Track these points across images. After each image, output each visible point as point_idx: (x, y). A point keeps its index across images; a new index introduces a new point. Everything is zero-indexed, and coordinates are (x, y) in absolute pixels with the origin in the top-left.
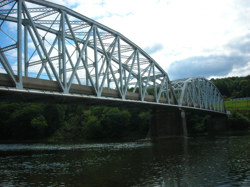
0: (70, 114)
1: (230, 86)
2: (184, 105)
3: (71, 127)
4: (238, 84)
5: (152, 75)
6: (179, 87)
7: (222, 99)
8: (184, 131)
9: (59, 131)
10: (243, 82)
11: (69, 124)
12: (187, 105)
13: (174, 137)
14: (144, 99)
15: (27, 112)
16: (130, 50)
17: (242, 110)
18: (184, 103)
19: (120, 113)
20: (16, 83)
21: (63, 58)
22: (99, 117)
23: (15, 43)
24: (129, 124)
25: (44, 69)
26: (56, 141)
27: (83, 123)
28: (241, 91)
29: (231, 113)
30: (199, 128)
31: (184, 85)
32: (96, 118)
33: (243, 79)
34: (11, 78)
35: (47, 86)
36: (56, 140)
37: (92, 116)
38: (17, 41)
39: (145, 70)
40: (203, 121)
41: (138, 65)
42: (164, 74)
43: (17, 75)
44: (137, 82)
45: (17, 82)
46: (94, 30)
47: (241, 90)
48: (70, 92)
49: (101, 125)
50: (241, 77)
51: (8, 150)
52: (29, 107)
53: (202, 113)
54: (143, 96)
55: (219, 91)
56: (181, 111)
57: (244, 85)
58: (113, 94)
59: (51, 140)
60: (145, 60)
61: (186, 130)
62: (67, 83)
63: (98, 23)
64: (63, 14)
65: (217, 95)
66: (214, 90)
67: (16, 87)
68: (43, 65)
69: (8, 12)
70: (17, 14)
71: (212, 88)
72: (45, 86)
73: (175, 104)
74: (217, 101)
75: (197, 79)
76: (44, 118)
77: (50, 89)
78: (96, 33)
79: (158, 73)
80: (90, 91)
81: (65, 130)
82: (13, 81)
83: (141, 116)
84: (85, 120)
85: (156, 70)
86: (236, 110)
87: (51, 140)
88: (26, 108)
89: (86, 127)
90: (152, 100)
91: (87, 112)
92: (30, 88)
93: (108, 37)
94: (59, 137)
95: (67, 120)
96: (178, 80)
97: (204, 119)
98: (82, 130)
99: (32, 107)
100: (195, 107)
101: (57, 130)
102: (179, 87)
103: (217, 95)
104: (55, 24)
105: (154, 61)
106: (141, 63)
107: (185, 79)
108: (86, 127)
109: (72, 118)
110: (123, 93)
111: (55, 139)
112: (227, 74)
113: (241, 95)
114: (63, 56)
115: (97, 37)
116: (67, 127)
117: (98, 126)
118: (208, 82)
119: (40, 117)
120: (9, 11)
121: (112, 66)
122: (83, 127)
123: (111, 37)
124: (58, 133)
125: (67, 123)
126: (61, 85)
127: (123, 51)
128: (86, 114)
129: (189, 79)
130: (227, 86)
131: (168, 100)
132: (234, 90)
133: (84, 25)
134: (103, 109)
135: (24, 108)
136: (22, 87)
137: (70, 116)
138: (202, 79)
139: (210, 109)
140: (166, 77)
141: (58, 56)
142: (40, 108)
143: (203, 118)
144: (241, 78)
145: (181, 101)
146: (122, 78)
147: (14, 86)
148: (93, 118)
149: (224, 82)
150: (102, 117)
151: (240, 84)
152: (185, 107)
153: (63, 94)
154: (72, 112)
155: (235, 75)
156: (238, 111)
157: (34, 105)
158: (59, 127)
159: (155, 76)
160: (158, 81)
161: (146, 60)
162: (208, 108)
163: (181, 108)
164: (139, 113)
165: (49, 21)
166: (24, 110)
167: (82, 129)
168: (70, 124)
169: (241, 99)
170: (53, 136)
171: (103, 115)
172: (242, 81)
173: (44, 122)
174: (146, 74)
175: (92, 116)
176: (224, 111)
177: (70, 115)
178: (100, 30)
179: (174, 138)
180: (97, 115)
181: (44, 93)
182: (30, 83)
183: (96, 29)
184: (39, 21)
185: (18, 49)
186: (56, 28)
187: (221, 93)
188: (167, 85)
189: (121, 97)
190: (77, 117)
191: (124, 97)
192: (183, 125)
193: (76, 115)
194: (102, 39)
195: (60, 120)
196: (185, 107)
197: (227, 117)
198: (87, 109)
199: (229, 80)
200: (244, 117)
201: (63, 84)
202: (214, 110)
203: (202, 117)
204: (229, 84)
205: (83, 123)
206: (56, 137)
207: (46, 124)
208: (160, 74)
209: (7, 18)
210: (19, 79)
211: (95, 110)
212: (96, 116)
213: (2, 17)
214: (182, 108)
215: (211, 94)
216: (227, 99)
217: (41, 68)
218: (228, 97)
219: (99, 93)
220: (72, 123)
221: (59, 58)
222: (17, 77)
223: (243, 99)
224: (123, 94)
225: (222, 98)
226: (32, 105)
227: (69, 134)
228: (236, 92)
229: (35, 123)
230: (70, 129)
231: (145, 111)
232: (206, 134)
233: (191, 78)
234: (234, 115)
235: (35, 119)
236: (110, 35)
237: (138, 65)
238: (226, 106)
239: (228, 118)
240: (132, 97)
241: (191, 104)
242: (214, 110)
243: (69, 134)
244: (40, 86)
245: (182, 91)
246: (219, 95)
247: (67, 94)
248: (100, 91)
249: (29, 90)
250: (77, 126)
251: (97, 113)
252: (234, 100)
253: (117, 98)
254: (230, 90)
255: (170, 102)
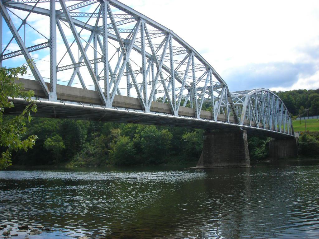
0: (93, 133)
1: (296, 101)
2: (246, 124)
3: (94, 149)
4: (307, 99)
5: (209, 85)
6: (240, 101)
7: (290, 118)
8: (246, 157)
9: (80, 155)
10: (314, 97)
11: (92, 146)
12: (250, 124)
13: (233, 165)
14: (200, 115)
15: (40, 130)
16: (183, 52)
17: (313, 132)
18: (246, 122)
19: (158, 133)
20: (49, 93)
21: (105, 61)
22: (132, 137)
23: (47, 41)
24: (170, 147)
25: (76, 75)
26: (76, 167)
27: (111, 145)
28: (310, 108)
29: (300, 135)
30: (259, 154)
31: (246, 99)
32: (128, 139)
33: (313, 93)
34: (42, 86)
35: (85, 98)
36: (76, 165)
37: (122, 136)
38: (49, 38)
39: (200, 79)
40: (264, 145)
41: (193, 72)
42: (223, 85)
43: (50, 82)
44: (188, 94)
45: (50, 92)
46: (141, 26)
47: (311, 106)
48: (113, 106)
49: (133, 148)
50: (310, 91)
51: (53, 171)
52: (42, 124)
53: (263, 135)
54: (199, 112)
55: (287, 108)
56: (242, 132)
57: (314, 100)
58: (163, 109)
59: (69, 166)
60: (200, 66)
61: (249, 157)
62: (110, 94)
63: (146, 17)
64: (105, 4)
65: (284, 112)
66: (280, 106)
67: (48, 98)
68: (75, 70)
69: (90, 15)
70: (49, 3)
71: (278, 102)
72: (82, 98)
73: (236, 123)
74: (283, 119)
75: (261, 91)
76: (61, 138)
77: (89, 102)
78: (144, 31)
79: (216, 83)
80: (137, 104)
81: (87, 153)
82: (44, 91)
83: (185, 137)
84: (114, 142)
85: (214, 79)
86: (306, 132)
87: (70, 166)
88: (38, 125)
89: (115, 150)
90: (208, 118)
91: (116, 131)
92: (66, 100)
93: (157, 35)
94: (80, 163)
95: (89, 141)
96: (237, 92)
97: (265, 143)
98: (109, 154)
99: (45, 124)
100: (258, 127)
101: (76, 154)
102: (240, 102)
103: (284, 112)
104: (40, 2)
105: (212, 68)
106: (197, 70)
107: (248, 91)
108: (115, 150)
109: (96, 139)
110: (176, 108)
111: (75, 164)
112: (290, 85)
113: (310, 113)
114: (105, 58)
115: (145, 35)
116: (90, 150)
117: (130, 149)
118: (273, 95)
119: (56, 136)
120: (92, 14)
121: (163, 74)
122: (111, 151)
123: (161, 36)
124: (79, 158)
125: (90, 144)
126: (102, 97)
127: (175, 54)
128: (115, 133)
129: (252, 92)
130: (292, 101)
131: (227, 117)
132: (302, 107)
133: (129, 20)
134: (136, 128)
135: (36, 125)
136: (57, 98)
137: (94, 136)
138: (267, 91)
139: (275, 130)
140: (225, 88)
141: (93, 60)
142: (56, 125)
143: (264, 141)
144: (311, 91)
145: (242, 119)
146: (107, 83)
147: (46, 96)
148: (124, 140)
149: (288, 96)
150: (135, 138)
151: (309, 99)
152: (247, 126)
153: (106, 109)
154: (96, 131)
155: (302, 88)
156: (308, 132)
157: (48, 121)
158: (79, 149)
159: (213, 86)
160: (216, 94)
161: (202, 66)
162: (273, 128)
163: (242, 128)
164: (182, 133)
165: (88, 14)
166: (36, 127)
167: (110, 152)
168: (93, 146)
169: (310, 117)
170: (72, 161)
171: (136, 135)
172: (312, 95)
173: (61, 143)
174: (201, 84)
175: (122, 136)
176: (291, 133)
177: (93, 135)
178: (149, 27)
179: (234, 166)
180: (129, 135)
181: (82, 106)
182: (65, 93)
183: (145, 25)
184: (72, 13)
185: (51, 49)
186: (92, 22)
187: (288, 109)
188: (226, 98)
189: (173, 113)
190: (103, 137)
191: (176, 113)
192: (245, 150)
193: (102, 134)
194: (151, 37)
195: (81, 141)
196: (247, 126)
197: (295, 140)
198: (116, 128)
199: (295, 93)
200: (316, 141)
201: (105, 94)
202: (280, 132)
203: (262, 141)
204: (295, 99)
205: (111, 145)
206: (76, 163)
207: (63, 145)
208: (218, 84)
209: (35, 9)
210: (52, 88)
211: (126, 129)
212: (127, 136)
213: (25, 7)
214: (244, 128)
215: (277, 110)
216: (293, 118)
217: (73, 75)
218: (294, 115)
219: (148, 108)
220: (96, 144)
221: (94, 62)
222: (50, 86)
223: (313, 118)
224: (176, 110)
225: (289, 117)
226: (46, 121)
227: (92, 159)
228: (304, 109)
229: (49, 144)
230: (93, 152)
231: (190, 131)
232: (268, 161)
233: (254, 91)
234: (304, 139)
235: (49, 139)
236: (159, 34)
237: (193, 72)
238: (294, 127)
239: (296, 142)
240: (186, 113)
241: (253, 123)
242: (280, 132)
243: (92, 158)
244: (77, 97)
245: (243, 107)
246: (286, 112)
247: (110, 108)
248: (149, 105)
249: (64, 102)
250: (103, 149)
251: (129, 132)
252: (302, 119)
253: (169, 114)
254: (296, 107)
255: (230, 120)
